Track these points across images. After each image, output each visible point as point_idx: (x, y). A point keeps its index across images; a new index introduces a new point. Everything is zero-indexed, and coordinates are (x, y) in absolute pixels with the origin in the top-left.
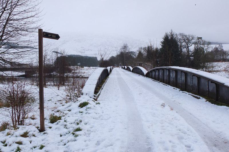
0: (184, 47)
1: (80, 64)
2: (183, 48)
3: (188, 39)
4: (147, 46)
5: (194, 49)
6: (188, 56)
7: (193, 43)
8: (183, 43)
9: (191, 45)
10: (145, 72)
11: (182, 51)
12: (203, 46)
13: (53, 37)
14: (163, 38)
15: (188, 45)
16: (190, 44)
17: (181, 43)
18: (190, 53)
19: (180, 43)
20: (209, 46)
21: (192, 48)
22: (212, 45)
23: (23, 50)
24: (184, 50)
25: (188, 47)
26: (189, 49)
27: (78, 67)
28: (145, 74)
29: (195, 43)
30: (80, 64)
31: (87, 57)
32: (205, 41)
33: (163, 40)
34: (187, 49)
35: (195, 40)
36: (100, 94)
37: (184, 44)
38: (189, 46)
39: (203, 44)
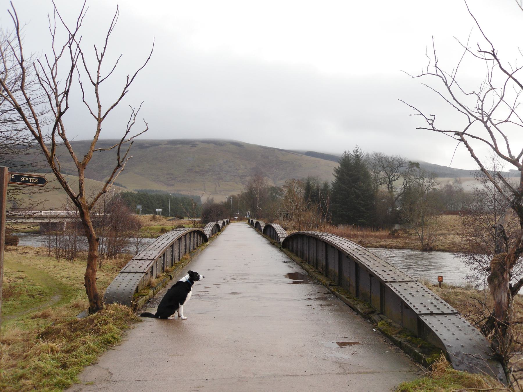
0: (382, 181)
1: (160, 210)
2: (381, 183)
3: (140, 225)
4: (306, 177)
5: (403, 186)
6: (392, 202)
7: (401, 174)
8: (381, 172)
9: (396, 177)
10: (282, 234)
11: (377, 191)
12: (421, 180)
13: (32, 183)
14: (339, 161)
15: (391, 177)
16: (394, 176)
17: (377, 173)
18: (396, 194)
19: (374, 172)
20: (433, 181)
21: (399, 185)
22: (439, 179)
23: (32, 174)
24: (383, 188)
25: (390, 182)
26: (392, 187)
27: (157, 216)
28: (282, 240)
29: (405, 175)
30: (160, 210)
31: (314, 152)
32: (425, 172)
33: (339, 165)
34: (388, 185)
35: (404, 168)
36: (365, 263)
37: (382, 174)
38: (393, 179)
39: (421, 177)
